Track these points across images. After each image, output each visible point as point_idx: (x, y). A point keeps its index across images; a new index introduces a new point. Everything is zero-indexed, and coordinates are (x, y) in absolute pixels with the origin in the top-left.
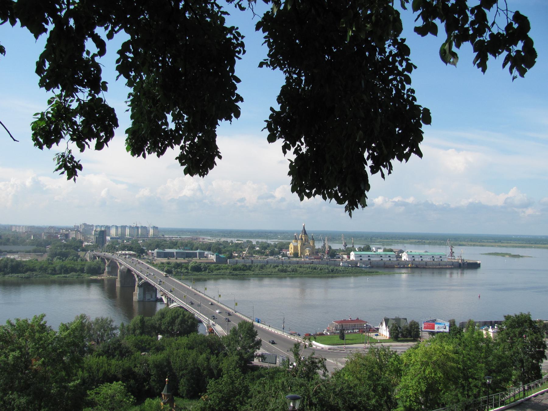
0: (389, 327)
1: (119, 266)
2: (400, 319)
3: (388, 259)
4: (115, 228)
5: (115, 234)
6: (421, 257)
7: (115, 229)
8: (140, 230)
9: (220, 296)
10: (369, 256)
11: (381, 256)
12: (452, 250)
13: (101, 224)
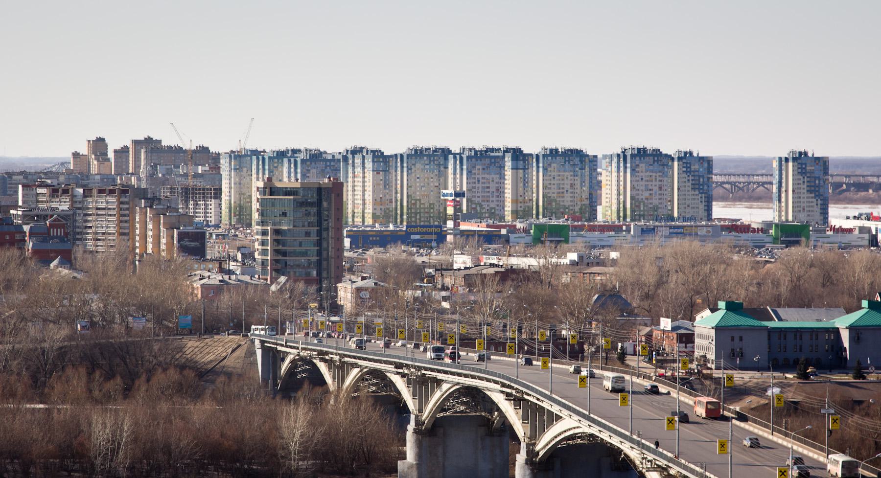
1: (520, 429)
4: (369, 165)
5: (369, 210)
7: (369, 175)
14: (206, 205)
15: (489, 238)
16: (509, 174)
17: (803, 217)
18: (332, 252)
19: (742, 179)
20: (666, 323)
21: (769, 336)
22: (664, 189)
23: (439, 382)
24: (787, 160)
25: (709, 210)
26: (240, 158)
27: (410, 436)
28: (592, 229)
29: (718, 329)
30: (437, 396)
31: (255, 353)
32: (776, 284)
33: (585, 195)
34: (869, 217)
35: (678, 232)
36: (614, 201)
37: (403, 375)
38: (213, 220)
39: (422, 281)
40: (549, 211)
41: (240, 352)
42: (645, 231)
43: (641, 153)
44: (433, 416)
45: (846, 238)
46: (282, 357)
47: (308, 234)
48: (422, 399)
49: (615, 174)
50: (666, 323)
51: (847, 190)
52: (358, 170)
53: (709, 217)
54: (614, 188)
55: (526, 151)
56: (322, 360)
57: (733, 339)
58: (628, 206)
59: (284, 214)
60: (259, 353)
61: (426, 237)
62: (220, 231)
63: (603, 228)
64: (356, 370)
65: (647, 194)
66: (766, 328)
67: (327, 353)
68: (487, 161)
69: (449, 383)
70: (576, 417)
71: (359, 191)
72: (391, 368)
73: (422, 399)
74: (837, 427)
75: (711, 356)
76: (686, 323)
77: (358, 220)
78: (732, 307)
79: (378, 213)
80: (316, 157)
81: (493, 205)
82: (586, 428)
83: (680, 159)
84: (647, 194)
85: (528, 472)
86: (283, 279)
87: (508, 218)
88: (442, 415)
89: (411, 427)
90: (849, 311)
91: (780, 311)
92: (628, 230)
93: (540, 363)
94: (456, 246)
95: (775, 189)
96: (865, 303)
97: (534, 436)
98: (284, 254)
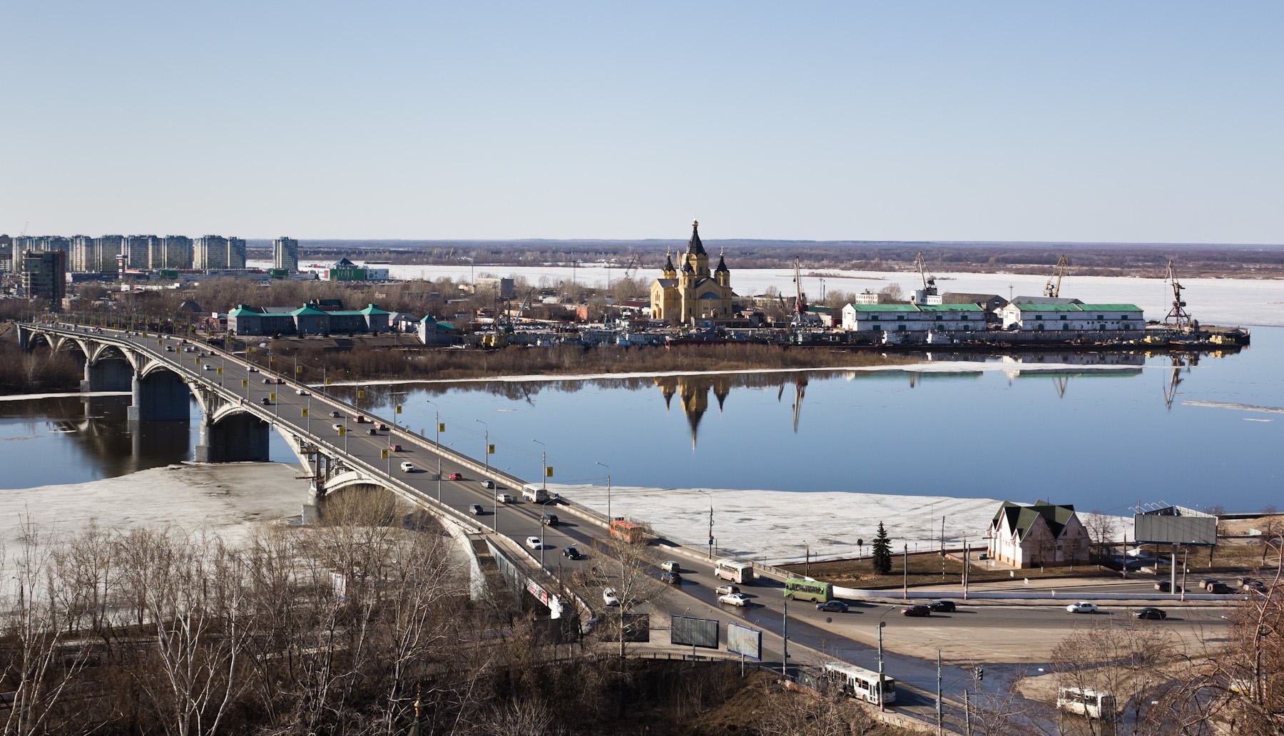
0: (1020, 532)
1: (134, 364)
2: (1053, 508)
3: (1060, 325)
4: (83, 243)
5: (84, 264)
6: (1063, 318)
7: (84, 248)
8: (164, 249)
9: (492, 448)
10: (901, 318)
11: (939, 318)
12: (1178, 295)
13: (36, 233)
14: (5, 262)
15: (138, 277)
16: (150, 247)
17: (286, 266)
18: (60, 284)
19: (262, 249)
20: (215, 315)
21: (262, 320)
22: (224, 253)
23: (99, 344)
24: (279, 241)
25: (296, 265)
26: (22, 241)
27: (86, 368)
28: (188, 272)
29: (238, 317)
30: (98, 350)
31: (17, 331)
32: (268, 296)
33: (187, 257)
34: (315, 266)
35: (228, 273)
36: (200, 260)
37: (83, 341)
38: (8, 269)
39: (105, 297)
40: (170, 265)
41: (9, 331)
42: (213, 273)
43: (212, 238)
44: (97, 359)
45: (304, 276)
46: (30, 332)
47: (48, 275)
48: (92, 351)
49: (200, 248)
50: (215, 315)
51: (310, 254)
52: (78, 246)
53: (244, 267)
54: (200, 253)
55: (158, 237)
56: (48, 334)
57: (245, 322)
58: (206, 262)
59: (36, 266)
60: (19, 331)
61: (110, 277)
62: (11, 274)
63: (194, 272)
64: (63, 339)
65: (215, 256)
66: (259, 316)
67: (49, 331)
68: (140, 241)
69: (104, 344)
70: (158, 359)
71: (79, 256)
72: (77, 337)
73: (92, 351)
74: (274, 361)
75: (235, 329)
76: (224, 315)
77: (78, 269)
78: (244, 307)
79: (88, 265)
80: (58, 240)
81: (143, 262)
82: (161, 364)
83: (230, 240)
84: (215, 256)
85: (138, 384)
86: (35, 297)
87: (150, 267)
88: (101, 359)
89: (87, 364)
90: (299, 308)
91: (267, 309)
92: (206, 273)
93: (141, 334)
94: (123, 281)
95: (274, 254)
96: (305, 305)
97: (141, 367)
98: (36, 285)
